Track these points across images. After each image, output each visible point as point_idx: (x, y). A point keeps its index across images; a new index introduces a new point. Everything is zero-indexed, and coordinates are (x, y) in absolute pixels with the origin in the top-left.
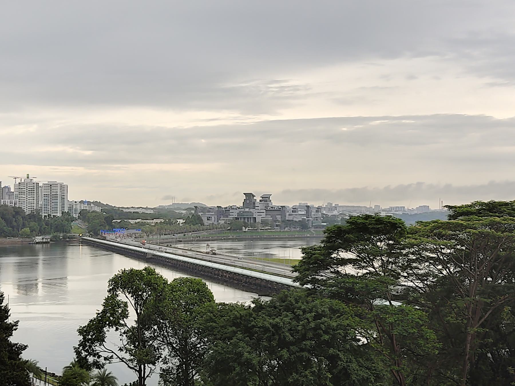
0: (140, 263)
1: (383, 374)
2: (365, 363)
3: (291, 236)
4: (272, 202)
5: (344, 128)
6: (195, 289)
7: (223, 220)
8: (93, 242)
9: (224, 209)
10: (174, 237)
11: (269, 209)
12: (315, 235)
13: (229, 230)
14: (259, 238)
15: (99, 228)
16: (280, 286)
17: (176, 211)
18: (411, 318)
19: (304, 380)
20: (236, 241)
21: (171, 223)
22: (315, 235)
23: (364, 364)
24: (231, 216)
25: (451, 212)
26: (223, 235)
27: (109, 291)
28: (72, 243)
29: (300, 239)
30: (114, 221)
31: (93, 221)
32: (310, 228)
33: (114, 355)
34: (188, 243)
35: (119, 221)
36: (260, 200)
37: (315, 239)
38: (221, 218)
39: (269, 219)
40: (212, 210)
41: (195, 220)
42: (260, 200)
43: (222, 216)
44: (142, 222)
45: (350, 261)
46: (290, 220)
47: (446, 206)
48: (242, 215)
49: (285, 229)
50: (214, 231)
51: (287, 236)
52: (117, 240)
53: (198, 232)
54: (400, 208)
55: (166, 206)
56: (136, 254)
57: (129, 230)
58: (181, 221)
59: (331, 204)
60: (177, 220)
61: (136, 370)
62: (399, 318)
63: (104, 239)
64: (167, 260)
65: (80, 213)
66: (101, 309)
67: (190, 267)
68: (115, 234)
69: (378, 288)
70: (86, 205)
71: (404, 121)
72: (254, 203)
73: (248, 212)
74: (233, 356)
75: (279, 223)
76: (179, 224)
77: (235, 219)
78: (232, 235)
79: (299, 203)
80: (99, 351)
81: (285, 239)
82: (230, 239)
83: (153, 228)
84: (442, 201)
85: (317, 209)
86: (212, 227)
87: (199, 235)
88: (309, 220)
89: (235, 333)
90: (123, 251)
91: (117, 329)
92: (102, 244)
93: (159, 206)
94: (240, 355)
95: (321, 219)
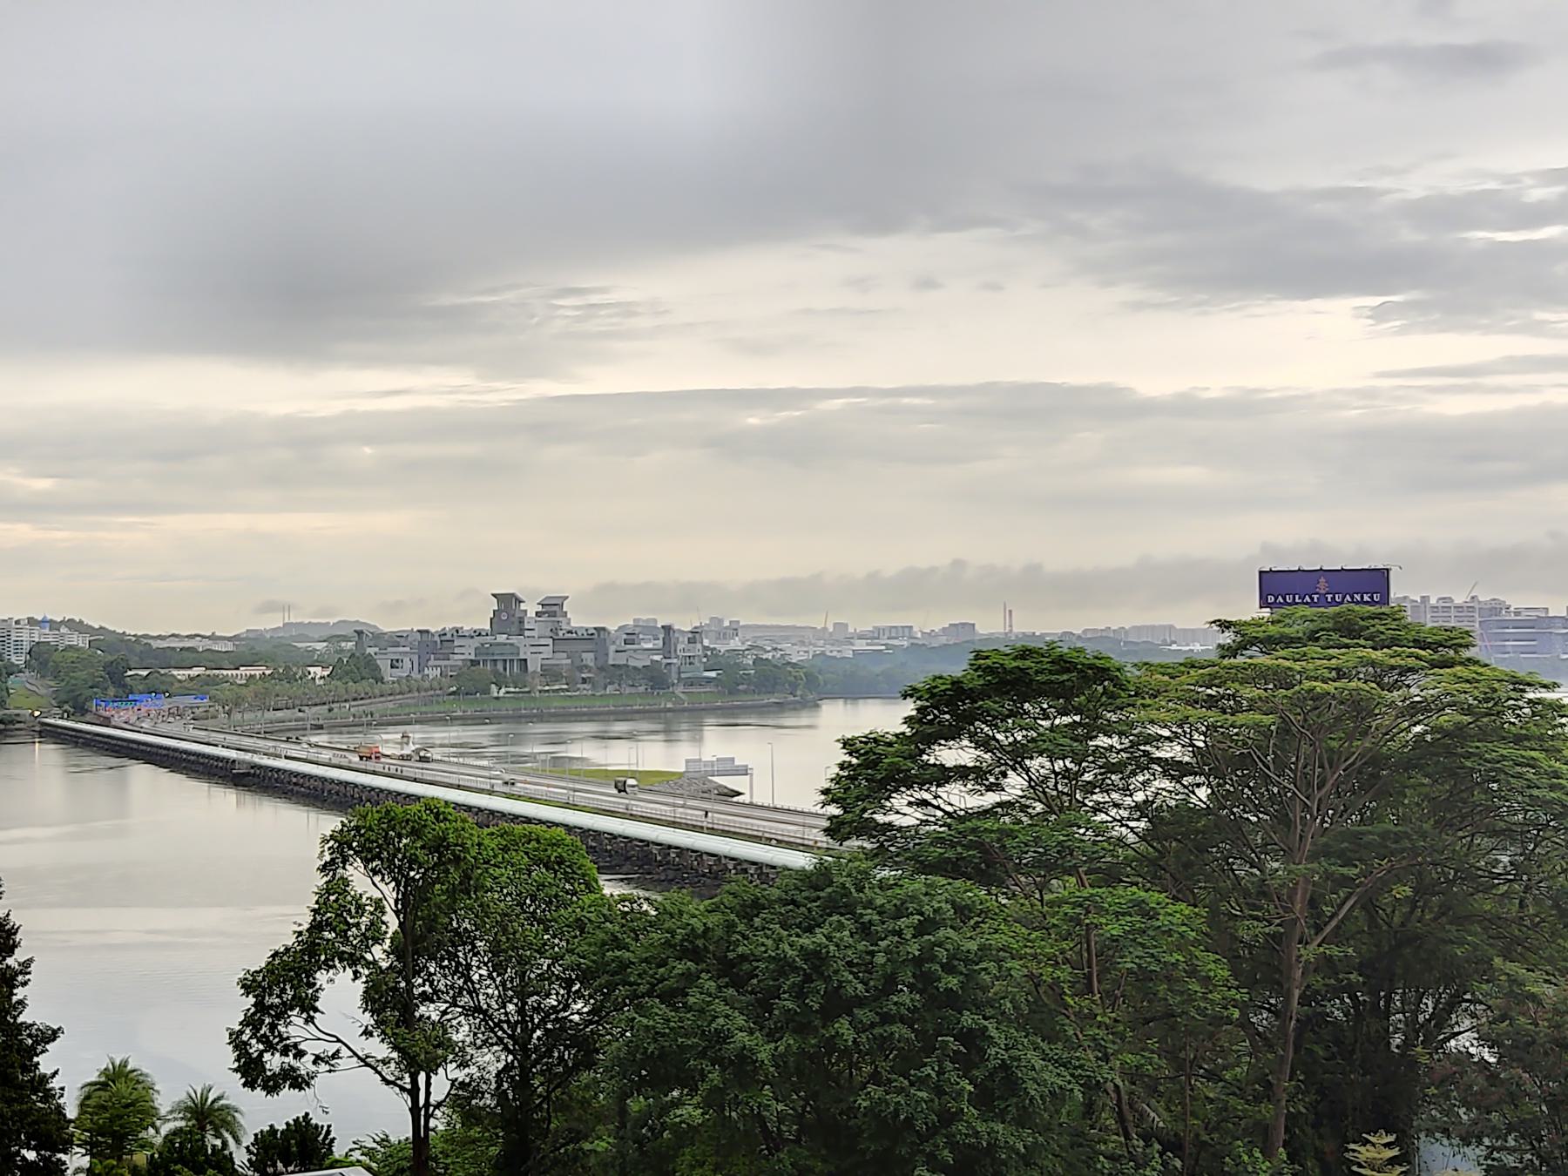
0: (212, 789)
1: (1103, 1078)
2: (1051, 1050)
3: (621, 708)
4: (569, 616)
5: (751, 416)
6: (553, 859)
7: (436, 667)
8: (74, 733)
9: (437, 638)
10: (301, 714)
11: (561, 636)
12: (686, 705)
13: (453, 693)
14: (535, 716)
15: (89, 692)
16: (622, 845)
17: (299, 645)
18: (1167, 923)
19: (903, 1102)
20: (486, 724)
21: (291, 679)
22: (686, 705)
23: (1048, 1051)
24: (456, 657)
25: (1228, 638)
26: (436, 708)
27: (323, 868)
28: (12, 736)
29: (647, 715)
30: (130, 673)
31: (72, 674)
32: (673, 685)
33: (344, 1048)
34: (341, 733)
35: (145, 673)
36: (537, 613)
37: (686, 714)
38: (430, 663)
39: (564, 662)
40: (403, 639)
41: (358, 669)
42: (537, 613)
43: (432, 656)
44: (209, 676)
45: (962, 773)
46: (619, 666)
47: (1214, 622)
48: (488, 654)
49: (605, 689)
50: (414, 698)
51: (612, 708)
52: (143, 725)
53: (369, 701)
54: (900, 630)
55: (267, 631)
56: (202, 764)
57: (174, 699)
58: (317, 671)
59: (720, 621)
60: (309, 669)
61: (402, 1089)
62: (1134, 925)
63: (106, 723)
64: (294, 780)
65: (29, 653)
66: (306, 920)
67: (361, 798)
68: (136, 708)
69: (1070, 843)
70: (47, 631)
71: (906, 400)
72: (521, 622)
73: (505, 644)
74: (695, 1040)
75: (589, 672)
76: (313, 679)
77: (469, 664)
78: (463, 708)
79: (634, 620)
80: (298, 1039)
81: (607, 718)
82: (456, 718)
83: (244, 691)
84: (1010, 611)
85: (690, 635)
86: (407, 687)
87: (372, 708)
88: (670, 664)
89: (690, 978)
90: (165, 755)
91: (356, 975)
92: (100, 739)
93: (248, 631)
94: (722, 1037)
95: (700, 661)
